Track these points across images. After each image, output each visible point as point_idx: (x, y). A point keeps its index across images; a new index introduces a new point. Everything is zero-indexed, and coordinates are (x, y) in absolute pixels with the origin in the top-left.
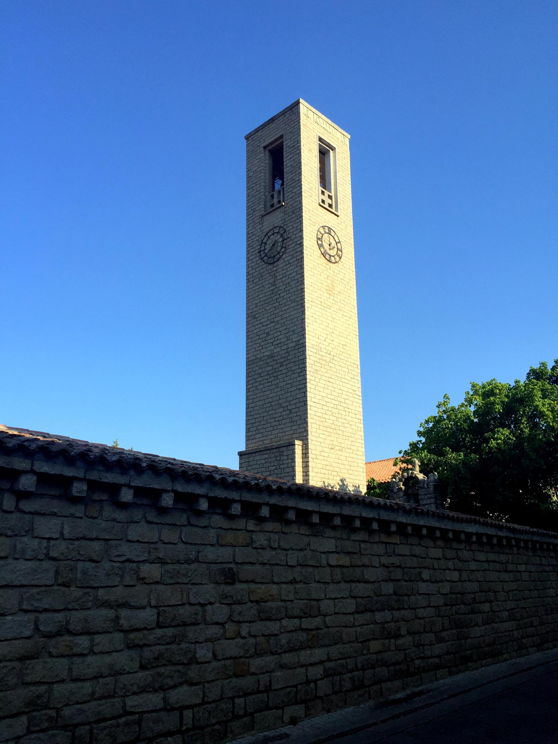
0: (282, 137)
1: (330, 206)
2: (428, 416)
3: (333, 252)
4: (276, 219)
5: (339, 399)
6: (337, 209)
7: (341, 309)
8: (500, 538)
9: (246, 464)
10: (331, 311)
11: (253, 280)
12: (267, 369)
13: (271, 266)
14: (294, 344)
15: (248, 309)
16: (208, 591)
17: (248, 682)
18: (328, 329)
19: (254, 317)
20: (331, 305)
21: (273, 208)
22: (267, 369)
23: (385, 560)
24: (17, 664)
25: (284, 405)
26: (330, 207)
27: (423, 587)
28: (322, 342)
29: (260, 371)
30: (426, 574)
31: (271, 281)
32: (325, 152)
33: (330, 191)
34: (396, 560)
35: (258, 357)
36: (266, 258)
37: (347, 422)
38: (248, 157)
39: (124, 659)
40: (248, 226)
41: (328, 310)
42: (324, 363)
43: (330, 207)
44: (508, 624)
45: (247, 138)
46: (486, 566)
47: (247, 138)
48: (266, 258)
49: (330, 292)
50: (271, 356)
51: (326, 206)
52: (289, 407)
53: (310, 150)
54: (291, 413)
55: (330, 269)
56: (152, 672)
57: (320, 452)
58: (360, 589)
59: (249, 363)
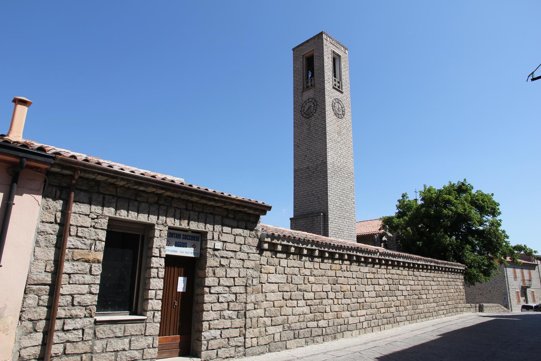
0: (313, 50)
1: (339, 87)
3: (341, 113)
4: (309, 94)
5: (344, 191)
6: (342, 89)
8: (431, 266)
9: (294, 225)
11: (297, 126)
12: (305, 175)
14: (320, 162)
15: (294, 142)
16: (328, 287)
17: (341, 321)
19: (298, 146)
21: (306, 88)
22: (305, 175)
23: (386, 276)
24: (279, 308)
25: (315, 194)
26: (338, 88)
27: (401, 287)
29: (301, 176)
30: (401, 282)
31: (308, 127)
32: (336, 59)
34: (390, 276)
35: (301, 168)
36: (304, 115)
38: (294, 60)
39: (306, 310)
40: (294, 97)
43: (338, 88)
44: (433, 304)
45: (293, 50)
46: (425, 278)
47: (293, 50)
48: (304, 115)
50: (308, 168)
51: (337, 88)
52: (318, 196)
53: (328, 58)
54: (319, 198)
56: (313, 314)
58: (377, 288)
59: (295, 171)
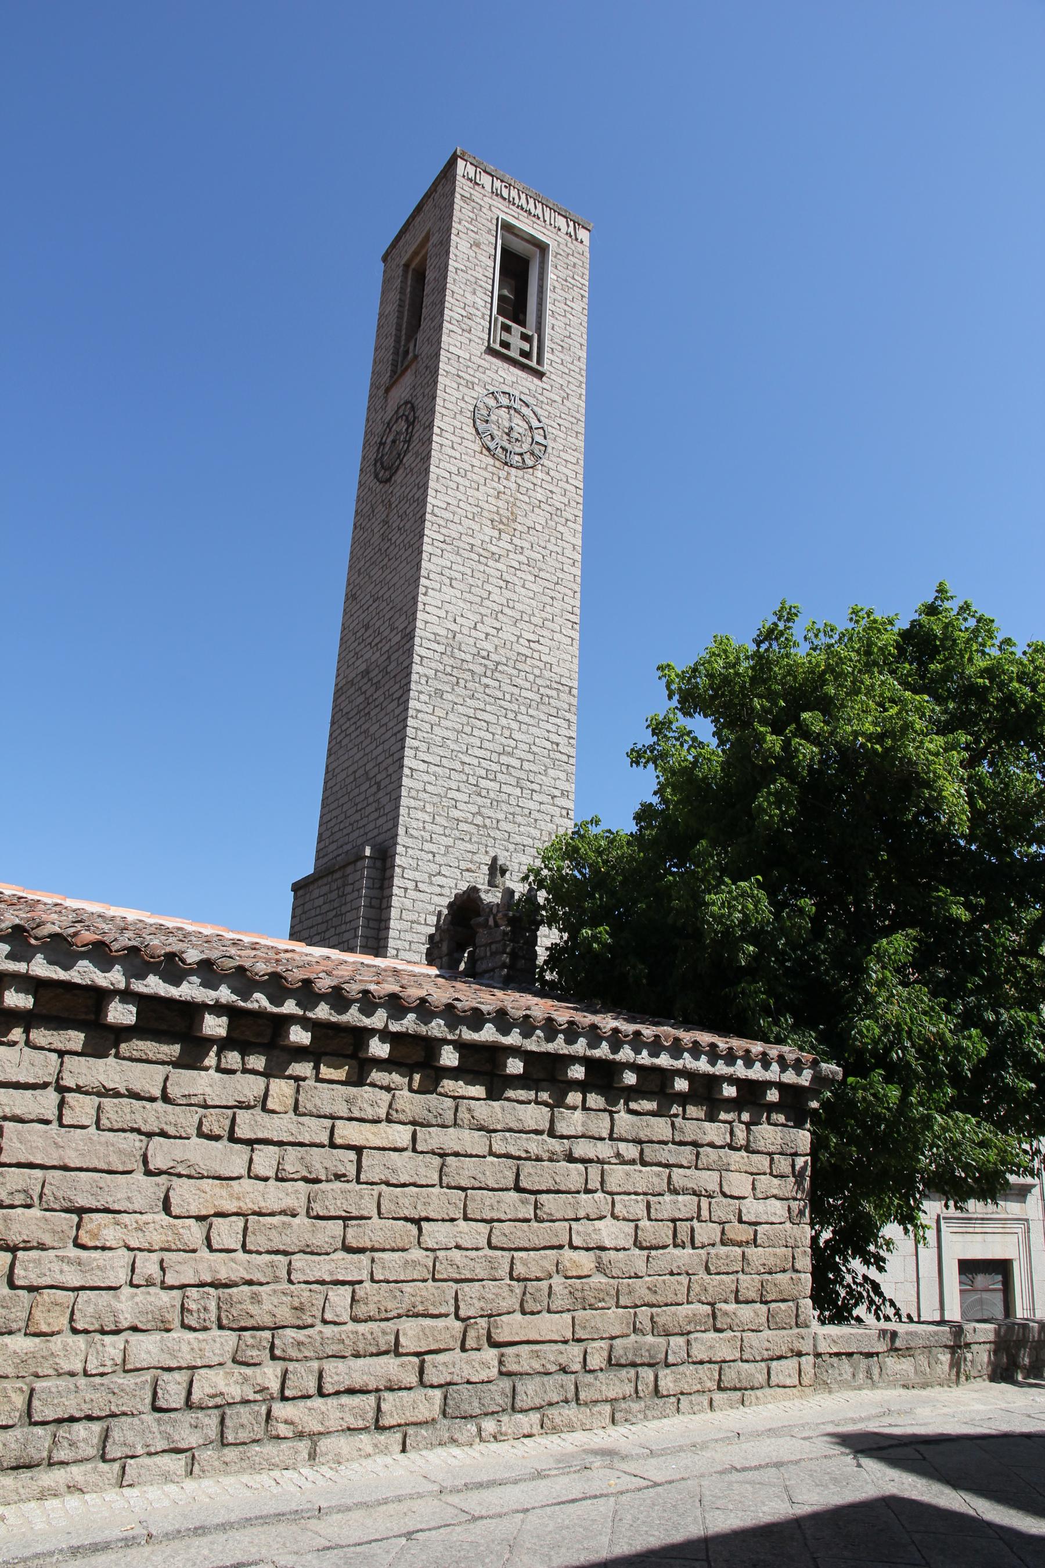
2: (696, 659)
6: (539, 362)
7: (564, 463)
10: (499, 565)
13: (388, 485)
18: (486, 603)
20: (504, 553)
28: (465, 631)
32: (519, 271)
33: (522, 323)
37: (527, 812)
41: (491, 563)
42: (467, 676)
49: (501, 526)
51: (514, 354)
55: (507, 479)
57: (431, 875)
